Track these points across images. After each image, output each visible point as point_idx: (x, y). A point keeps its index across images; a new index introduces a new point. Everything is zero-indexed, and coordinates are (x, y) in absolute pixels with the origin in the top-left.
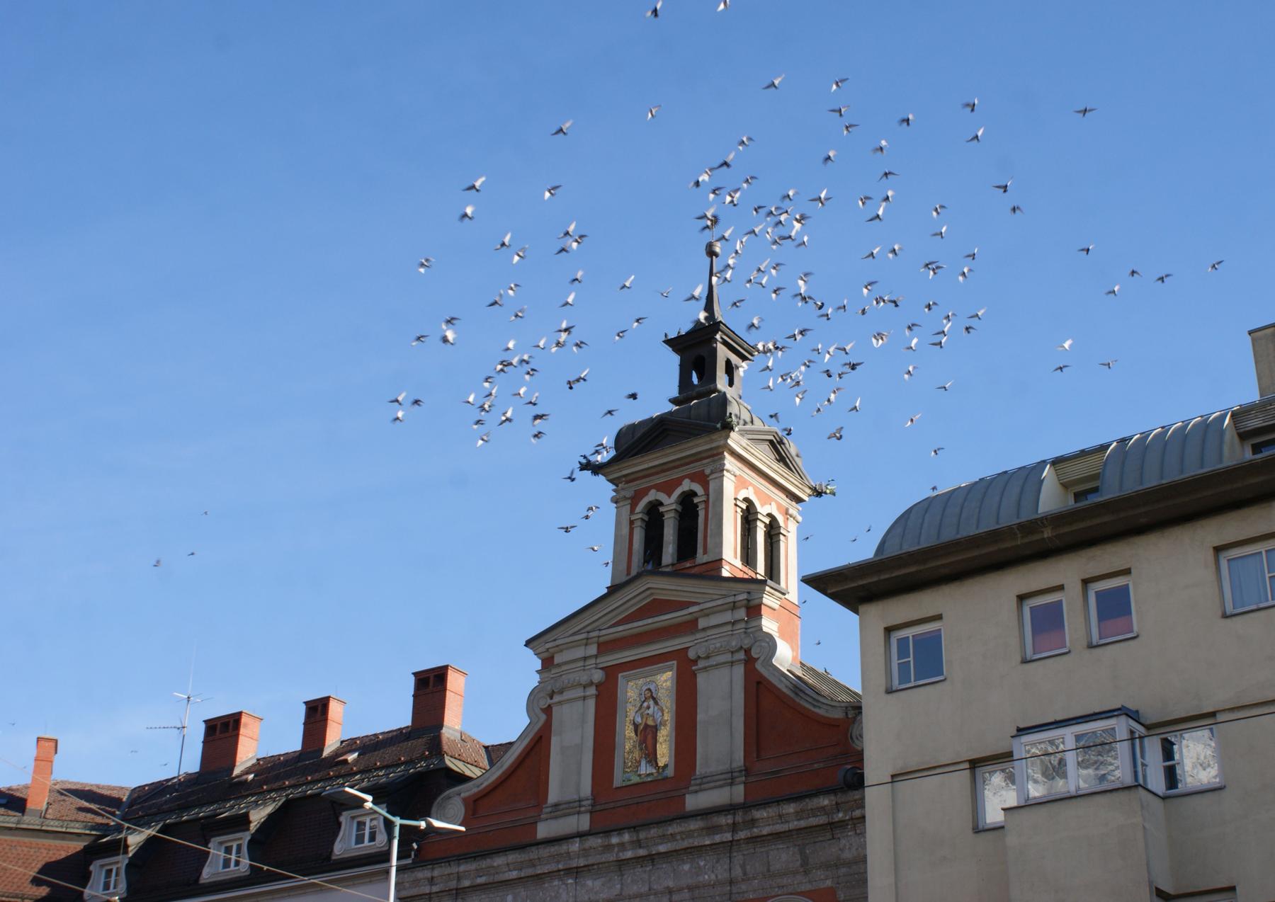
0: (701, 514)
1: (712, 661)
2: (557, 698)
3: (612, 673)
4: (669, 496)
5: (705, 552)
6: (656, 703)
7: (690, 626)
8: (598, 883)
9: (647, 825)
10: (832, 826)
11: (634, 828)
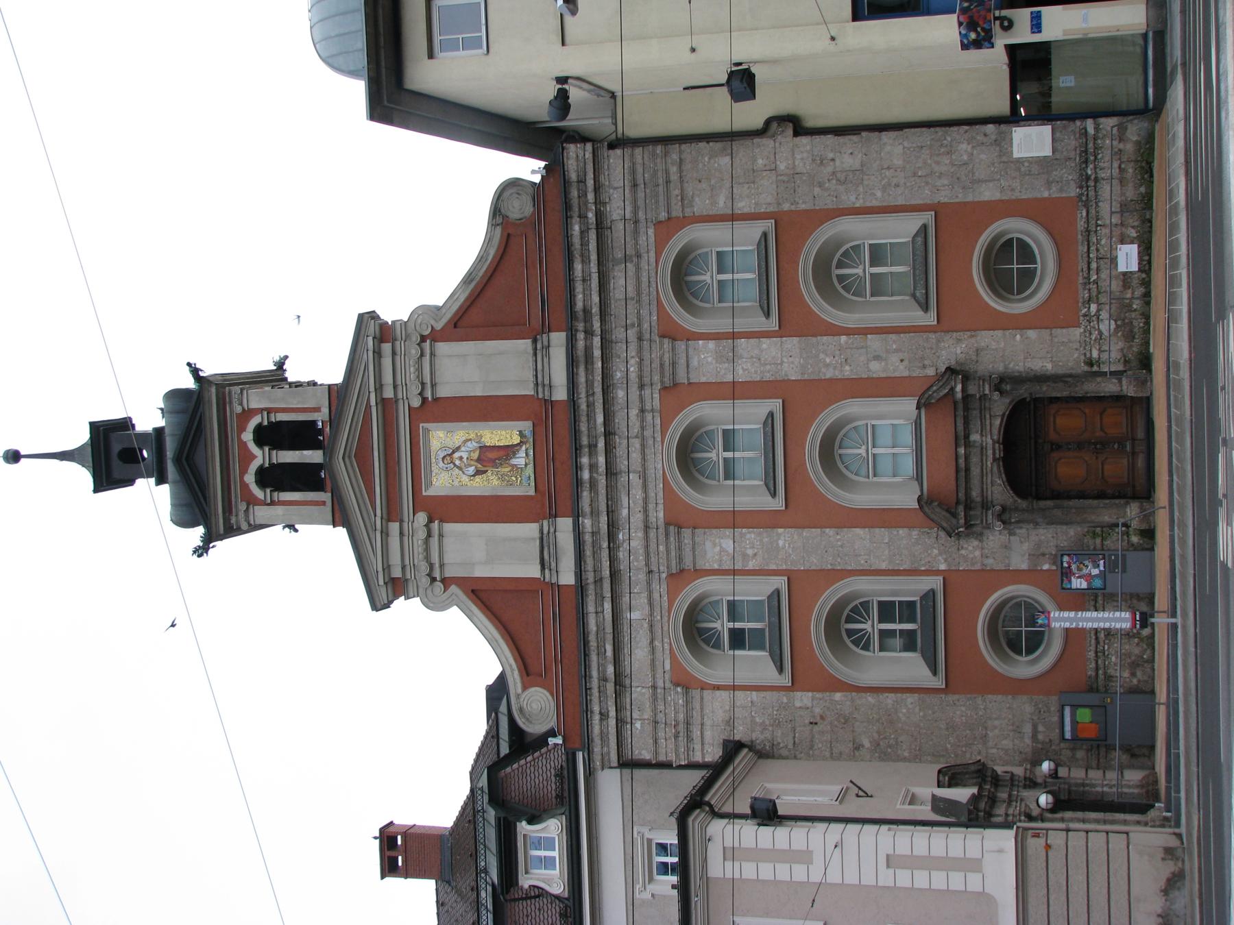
0: (282, 417)
1: (427, 380)
2: (437, 574)
3: (420, 503)
4: (255, 457)
5: (317, 410)
6: (458, 449)
7: (387, 407)
9: (576, 433)
10: (600, 226)
11: (578, 449)
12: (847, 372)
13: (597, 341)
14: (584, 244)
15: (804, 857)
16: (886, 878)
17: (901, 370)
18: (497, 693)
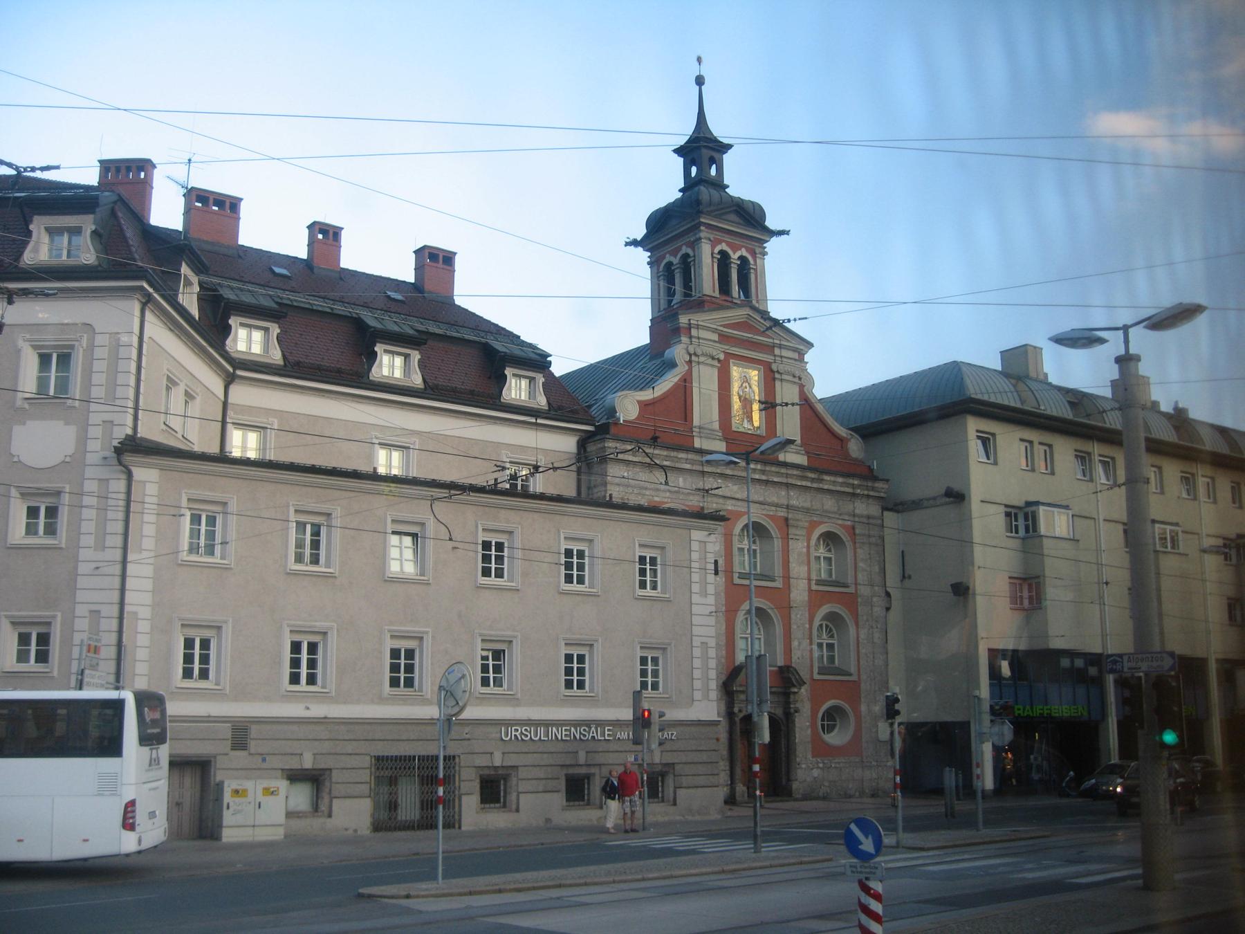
0: (753, 276)
7: (769, 348)
8: (735, 488)
12: (794, 627)
13: (809, 484)
14: (848, 485)
15: (101, 546)
16: (81, 610)
17: (794, 658)
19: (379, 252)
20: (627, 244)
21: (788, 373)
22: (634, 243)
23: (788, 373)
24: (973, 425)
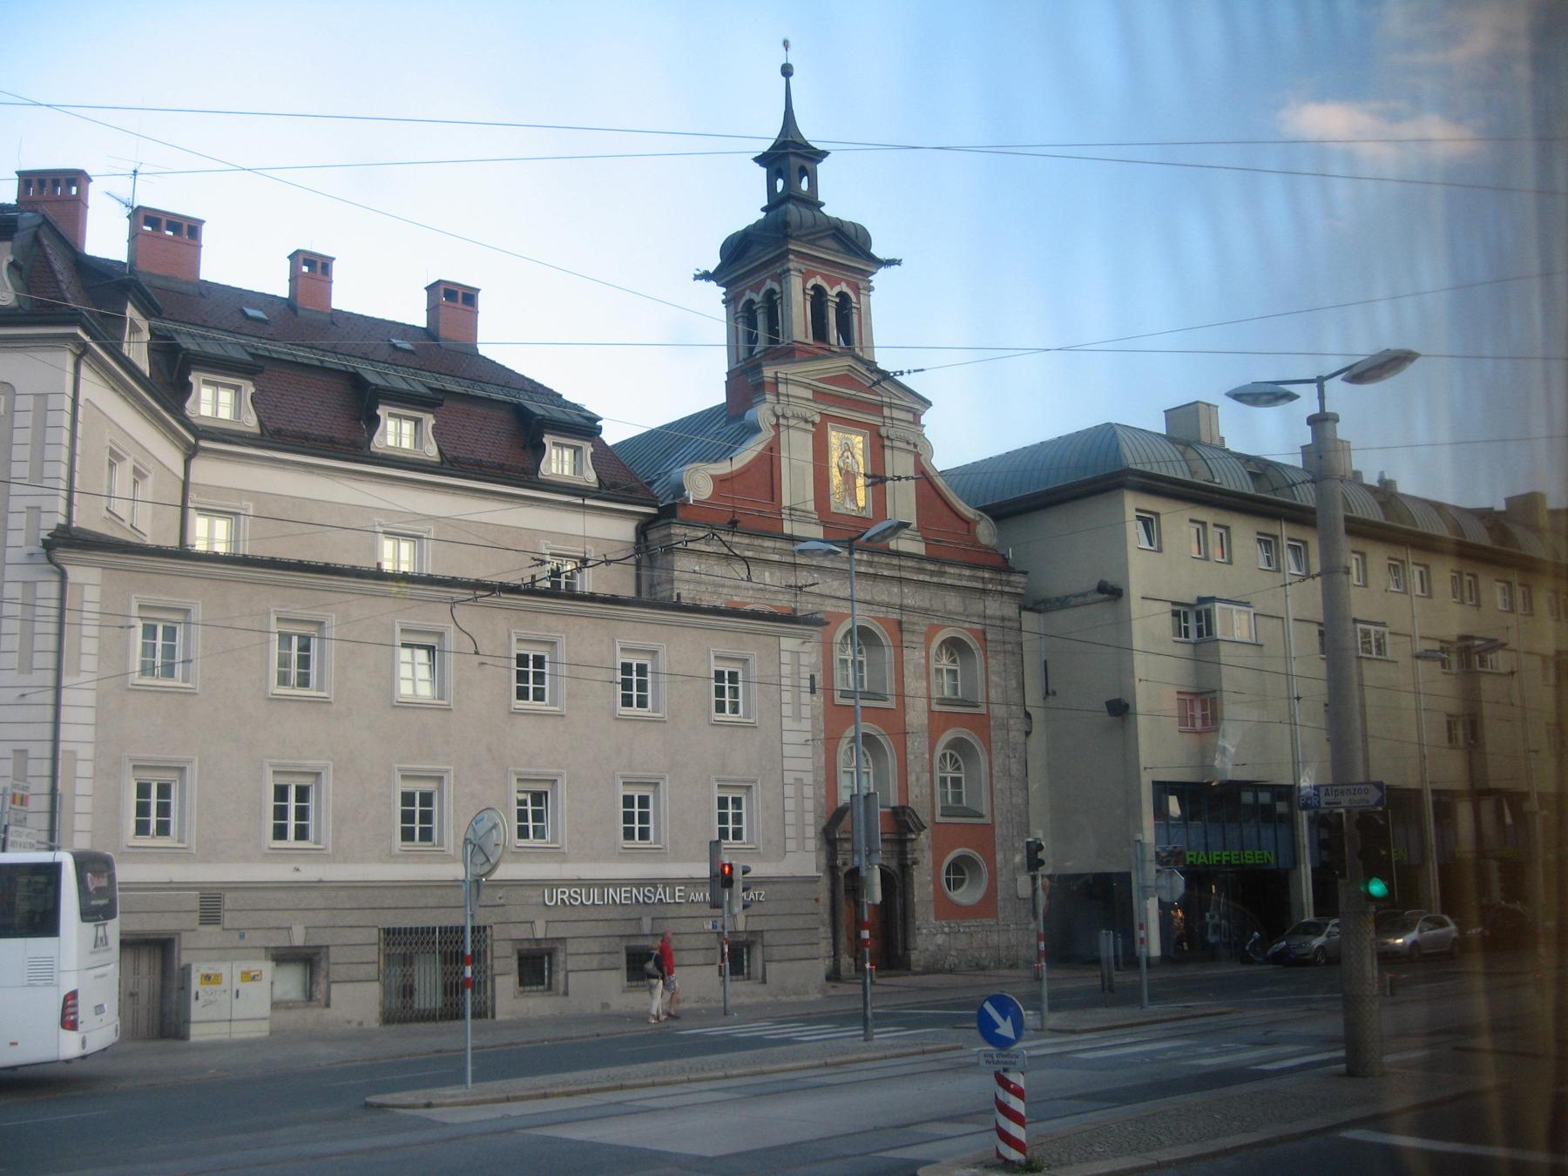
12: (910, 757)
13: (927, 578)
17: (912, 797)
18: (583, 427)
19: (380, 289)
20: (697, 277)
21: (900, 439)
22: (706, 276)
23: (900, 439)
24: (1132, 503)
